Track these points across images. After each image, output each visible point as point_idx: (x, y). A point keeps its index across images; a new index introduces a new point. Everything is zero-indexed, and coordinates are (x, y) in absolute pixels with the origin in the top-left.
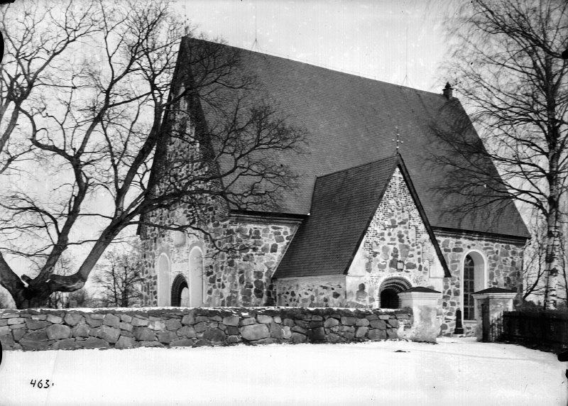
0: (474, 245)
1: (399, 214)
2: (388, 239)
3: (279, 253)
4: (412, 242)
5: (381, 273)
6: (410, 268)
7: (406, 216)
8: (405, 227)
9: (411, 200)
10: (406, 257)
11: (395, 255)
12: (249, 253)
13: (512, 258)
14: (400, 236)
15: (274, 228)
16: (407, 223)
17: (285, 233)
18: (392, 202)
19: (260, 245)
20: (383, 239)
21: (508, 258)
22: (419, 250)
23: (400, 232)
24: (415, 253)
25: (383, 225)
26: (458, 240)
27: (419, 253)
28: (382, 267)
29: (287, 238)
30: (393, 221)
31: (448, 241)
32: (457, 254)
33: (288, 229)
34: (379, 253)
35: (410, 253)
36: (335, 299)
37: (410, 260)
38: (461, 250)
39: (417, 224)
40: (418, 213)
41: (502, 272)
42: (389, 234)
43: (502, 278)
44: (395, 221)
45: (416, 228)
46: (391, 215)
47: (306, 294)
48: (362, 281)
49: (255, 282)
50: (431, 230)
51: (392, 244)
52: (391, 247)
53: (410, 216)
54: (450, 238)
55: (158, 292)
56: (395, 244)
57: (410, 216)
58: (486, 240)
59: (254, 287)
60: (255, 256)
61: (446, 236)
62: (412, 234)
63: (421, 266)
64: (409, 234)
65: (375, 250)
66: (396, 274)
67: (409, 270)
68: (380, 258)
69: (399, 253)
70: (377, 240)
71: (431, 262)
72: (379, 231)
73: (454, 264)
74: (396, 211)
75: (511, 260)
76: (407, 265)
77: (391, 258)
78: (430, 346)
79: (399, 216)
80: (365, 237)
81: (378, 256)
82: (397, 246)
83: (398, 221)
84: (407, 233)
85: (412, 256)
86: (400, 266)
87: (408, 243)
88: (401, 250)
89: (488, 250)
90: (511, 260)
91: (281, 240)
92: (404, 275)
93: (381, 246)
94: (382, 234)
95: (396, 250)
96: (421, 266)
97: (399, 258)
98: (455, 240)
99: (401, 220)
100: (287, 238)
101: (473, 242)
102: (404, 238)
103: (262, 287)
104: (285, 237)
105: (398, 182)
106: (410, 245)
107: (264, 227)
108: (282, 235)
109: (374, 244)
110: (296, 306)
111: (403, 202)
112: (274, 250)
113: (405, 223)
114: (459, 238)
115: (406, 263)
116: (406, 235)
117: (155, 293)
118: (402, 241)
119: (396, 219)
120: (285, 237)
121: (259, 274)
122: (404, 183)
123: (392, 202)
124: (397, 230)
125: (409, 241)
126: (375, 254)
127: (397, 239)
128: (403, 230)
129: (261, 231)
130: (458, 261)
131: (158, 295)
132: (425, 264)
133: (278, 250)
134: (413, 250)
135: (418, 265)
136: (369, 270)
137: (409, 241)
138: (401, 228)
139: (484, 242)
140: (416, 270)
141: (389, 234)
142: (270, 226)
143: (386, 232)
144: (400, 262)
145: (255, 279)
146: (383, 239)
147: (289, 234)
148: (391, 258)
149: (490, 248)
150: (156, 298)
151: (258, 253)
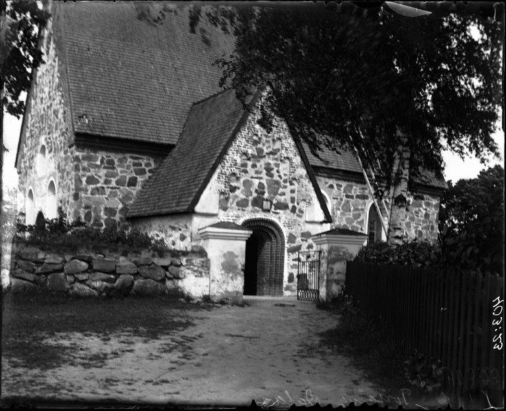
1: (267, 141)
2: (252, 172)
3: (138, 187)
4: (284, 177)
5: (240, 213)
6: (280, 209)
8: (276, 159)
10: (276, 193)
11: (260, 192)
12: (99, 185)
13: (426, 210)
14: (269, 169)
15: (132, 158)
16: (279, 154)
19: (114, 177)
20: (246, 172)
21: (421, 209)
22: (292, 187)
23: (270, 164)
24: (287, 191)
25: (245, 154)
27: (293, 191)
29: (150, 171)
30: (260, 151)
32: (361, 201)
33: (152, 162)
34: (239, 188)
36: (181, 243)
37: (282, 199)
40: (293, 143)
41: (413, 225)
43: (413, 231)
44: (263, 151)
46: (256, 143)
49: (106, 221)
51: (256, 178)
52: (256, 182)
54: (353, 184)
56: (261, 178)
59: (104, 226)
60: (106, 189)
61: (348, 181)
63: (294, 208)
64: (281, 168)
65: (234, 184)
66: (260, 215)
67: (278, 211)
68: (240, 194)
69: (266, 190)
70: (237, 171)
72: (239, 161)
73: (357, 212)
75: (424, 212)
76: (275, 205)
77: (255, 195)
78: (14, 165)
79: (267, 145)
80: (220, 166)
81: (238, 192)
82: (264, 181)
83: (266, 151)
84: (277, 165)
85: (284, 194)
86: (266, 205)
87: (278, 179)
88: (269, 187)
90: (424, 212)
91: (142, 172)
92: (271, 217)
93: (242, 180)
95: (261, 185)
96: (294, 208)
97: (266, 195)
99: (270, 150)
102: (274, 172)
106: (281, 181)
107: (120, 156)
108: (143, 166)
112: (133, 182)
113: (276, 154)
115: (274, 202)
116: (276, 169)
118: (272, 176)
119: (265, 148)
120: (147, 169)
121: (110, 211)
125: (280, 176)
126: (233, 189)
127: (265, 172)
128: (272, 162)
129: (116, 161)
130: (363, 210)
133: (138, 184)
134: (285, 187)
135: (290, 205)
136: (225, 209)
137: (280, 176)
140: (288, 211)
142: (128, 155)
143: (250, 163)
144: (267, 200)
145: (105, 217)
146: (246, 172)
148: (255, 195)
151: (111, 186)
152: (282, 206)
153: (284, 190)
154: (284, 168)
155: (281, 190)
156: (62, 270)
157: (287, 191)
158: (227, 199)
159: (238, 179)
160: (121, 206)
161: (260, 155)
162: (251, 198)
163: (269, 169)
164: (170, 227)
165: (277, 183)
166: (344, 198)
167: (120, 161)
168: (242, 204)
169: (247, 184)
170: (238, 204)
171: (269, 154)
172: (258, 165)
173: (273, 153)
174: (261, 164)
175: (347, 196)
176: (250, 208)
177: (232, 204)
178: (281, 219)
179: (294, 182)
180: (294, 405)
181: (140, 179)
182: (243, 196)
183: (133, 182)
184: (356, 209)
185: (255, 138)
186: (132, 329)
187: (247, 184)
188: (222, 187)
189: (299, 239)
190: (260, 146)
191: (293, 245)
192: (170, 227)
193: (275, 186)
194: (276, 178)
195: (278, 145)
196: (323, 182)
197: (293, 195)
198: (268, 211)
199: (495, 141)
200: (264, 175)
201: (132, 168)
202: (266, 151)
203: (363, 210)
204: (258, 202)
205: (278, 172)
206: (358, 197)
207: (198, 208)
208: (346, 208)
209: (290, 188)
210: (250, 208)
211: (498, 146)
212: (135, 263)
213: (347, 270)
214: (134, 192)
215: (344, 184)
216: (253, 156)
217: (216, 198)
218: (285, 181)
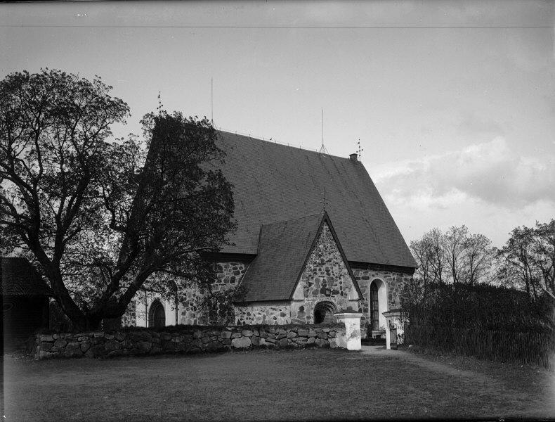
1: (326, 254)
2: (319, 274)
10: (332, 285)
15: (232, 264)
18: (321, 246)
20: (316, 273)
24: (338, 283)
28: (315, 293)
30: (323, 260)
33: (243, 266)
46: (320, 256)
47: (260, 314)
62: (336, 269)
63: (342, 292)
65: (310, 281)
70: (312, 274)
81: (313, 286)
84: (332, 268)
86: (328, 293)
91: (238, 273)
94: (315, 270)
95: (324, 281)
96: (342, 292)
111: (329, 246)
112: (233, 280)
118: (329, 275)
123: (321, 246)
124: (324, 267)
126: (310, 284)
130: (366, 287)
135: (340, 291)
136: (307, 297)
140: (339, 295)
141: (320, 270)
143: (318, 268)
146: (316, 273)
148: (321, 287)
152: (336, 292)
153: (336, 283)
154: (336, 269)
156: (286, 337)
157: (338, 283)
158: (308, 290)
159: (312, 278)
161: (323, 263)
162: (319, 289)
163: (328, 271)
165: (333, 279)
167: (226, 267)
168: (315, 293)
169: (317, 280)
171: (327, 262)
172: (322, 269)
173: (329, 261)
174: (324, 268)
176: (319, 295)
177: (310, 293)
178: (335, 299)
179: (342, 277)
180: (516, 231)
181: (237, 277)
182: (315, 288)
183: (233, 280)
185: (320, 253)
186: (400, 332)
187: (317, 280)
194: (332, 276)
195: (331, 256)
197: (342, 285)
198: (329, 295)
200: (325, 275)
201: (232, 271)
203: (366, 287)
204: (323, 291)
209: (339, 281)
210: (319, 295)
212: (316, 331)
217: (302, 290)
218: (336, 277)
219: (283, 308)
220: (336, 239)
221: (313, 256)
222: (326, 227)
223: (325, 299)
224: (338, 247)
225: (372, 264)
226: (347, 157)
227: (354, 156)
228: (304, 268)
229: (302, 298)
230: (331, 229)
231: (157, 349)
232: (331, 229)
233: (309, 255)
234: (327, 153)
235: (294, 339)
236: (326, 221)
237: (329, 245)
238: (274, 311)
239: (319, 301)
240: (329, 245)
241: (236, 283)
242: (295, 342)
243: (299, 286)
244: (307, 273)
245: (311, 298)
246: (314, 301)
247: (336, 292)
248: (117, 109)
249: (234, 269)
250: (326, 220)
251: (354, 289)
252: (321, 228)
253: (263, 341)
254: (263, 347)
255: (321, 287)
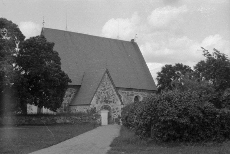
0: (138, 93)
1: (107, 86)
2: (103, 94)
3: (72, 97)
7: (109, 87)
9: (111, 82)
10: (109, 99)
14: (107, 93)
17: (74, 91)
18: (104, 83)
24: (112, 98)
25: (102, 90)
26: (132, 92)
27: (113, 98)
28: (101, 102)
29: (74, 92)
30: (105, 89)
31: (129, 92)
32: (132, 96)
33: (75, 90)
35: (110, 98)
37: (111, 100)
38: (133, 95)
39: (112, 89)
42: (104, 92)
45: (112, 90)
46: (104, 87)
47: (79, 110)
48: (95, 106)
50: (117, 89)
52: (104, 96)
53: (110, 87)
54: (129, 91)
55: (33, 109)
57: (110, 87)
58: (142, 92)
59: (64, 108)
62: (111, 92)
69: (107, 98)
71: (117, 100)
72: (100, 91)
74: (106, 86)
81: (100, 99)
82: (106, 96)
83: (106, 88)
85: (111, 99)
86: (168, 100)
87: (110, 95)
89: (143, 95)
91: (72, 93)
92: (109, 105)
93: (101, 96)
94: (101, 92)
95: (105, 97)
98: (131, 92)
99: (108, 88)
100: (74, 92)
101: (138, 92)
102: (109, 93)
103: (66, 108)
104: (74, 92)
105: (106, 77)
109: (99, 96)
110: (132, 93)
111: (108, 83)
112: (70, 96)
114: (133, 91)
117: (32, 109)
120: (74, 92)
122: (108, 77)
123: (104, 83)
124: (106, 91)
125: (110, 94)
126: (99, 98)
127: (106, 94)
131: (33, 110)
132: (116, 101)
134: (111, 97)
135: (113, 101)
136: (97, 103)
137: (110, 94)
138: (107, 90)
139: (141, 92)
140: (112, 103)
141: (104, 92)
143: (103, 92)
146: (102, 94)
147: (75, 91)
148: (104, 99)
149: (143, 94)
150: (32, 111)
155: (110, 98)
157: (112, 98)
160: (67, 102)
161: (105, 90)
163: (107, 93)
164: (83, 108)
165: (110, 96)
166: (127, 96)
168: (101, 102)
170: (100, 102)
174: (105, 92)
175: (128, 95)
176: (103, 103)
177: (99, 102)
179: (114, 95)
181: (72, 95)
182: (101, 100)
184: (130, 99)
185: (104, 85)
188: (97, 98)
189: (115, 110)
190: (105, 87)
191: (114, 111)
192: (83, 108)
193: (109, 97)
195: (109, 87)
196: (120, 92)
199: (190, 66)
200: (106, 94)
202: (106, 88)
205: (110, 93)
206: (131, 95)
207: (91, 103)
208: (127, 99)
210: (103, 103)
211: (191, 67)
213: (104, 39)
214: (71, 98)
215: (126, 92)
216: (104, 90)
217: (95, 101)
218: (111, 95)
219: (87, 107)
220: (111, 80)
221: (101, 87)
222: (106, 75)
223: (106, 104)
224: (112, 83)
225: (135, 89)
226: (130, 41)
227: (133, 40)
228: (96, 91)
229: (95, 104)
230: (109, 76)
231: (27, 123)
232: (109, 76)
233: (99, 86)
234: (120, 39)
235: (80, 120)
236: (107, 72)
237: (108, 82)
238: (84, 109)
239: (103, 105)
240: (108, 82)
241: (72, 97)
242: (80, 121)
243: (94, 99)
244: (97, 93)
245: (99, 104)
246: (101, 105)
247: (111, 102)
248: (3, 38)
249: (71, 91)
250: (107, 72)
251: (119, 100)
252: (104, 75)
253: (68, 121)
254: (67, 123)
255: (104, 99)
